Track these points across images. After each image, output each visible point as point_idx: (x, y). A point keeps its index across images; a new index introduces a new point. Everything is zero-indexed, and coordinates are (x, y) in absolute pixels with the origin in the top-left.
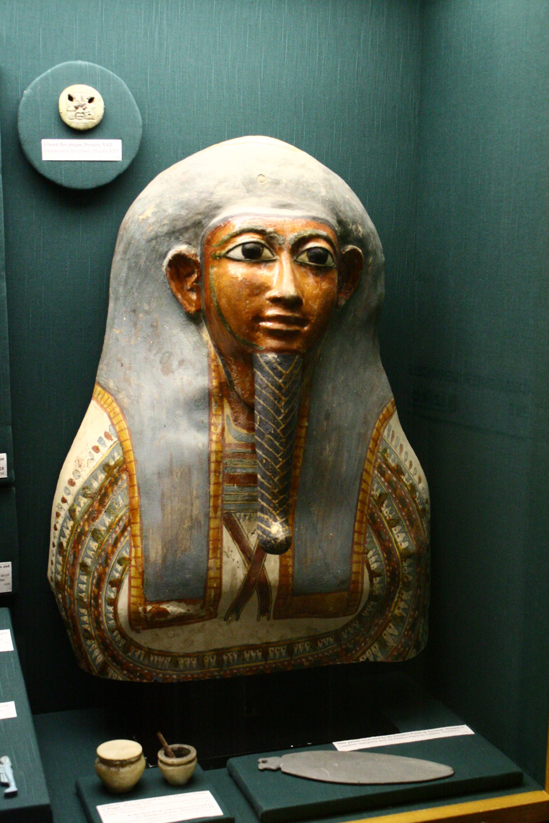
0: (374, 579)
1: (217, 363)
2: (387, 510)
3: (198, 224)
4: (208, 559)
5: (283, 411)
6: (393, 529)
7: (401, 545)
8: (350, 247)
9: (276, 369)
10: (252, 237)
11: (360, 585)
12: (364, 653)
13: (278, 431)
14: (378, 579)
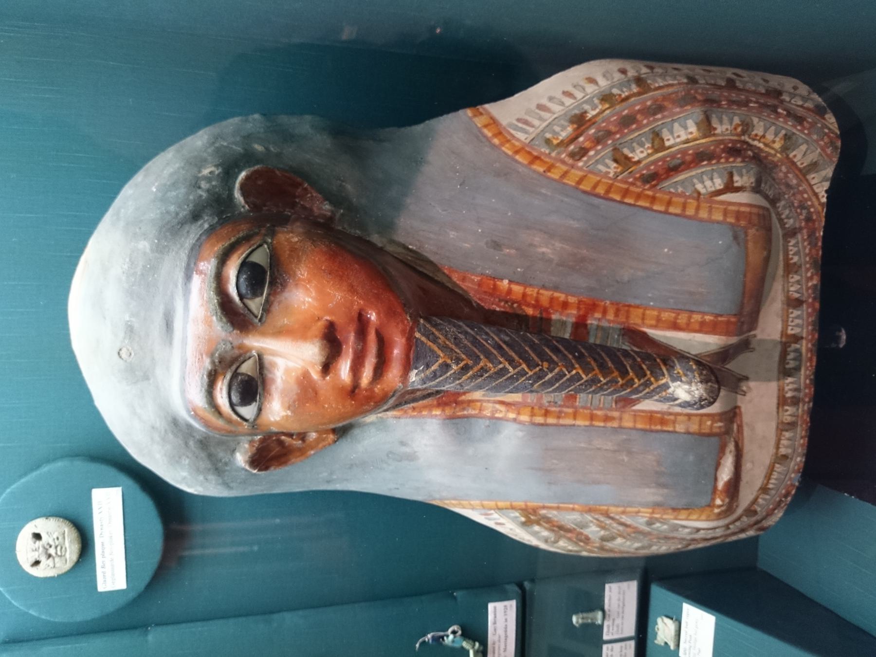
0: (736, 185)
1: (410, 408)
2: (638, 151)
3: (204, 444)
4: (675, 432)
5: (501, 366)
6: (667, 144)
7: (691, 133)
8: (237, 195)
9: (435, 372)
10: (221, 393)
11: (742, 209)
12: (816, 195)
13: (530, 373)
14: (736, 178)
